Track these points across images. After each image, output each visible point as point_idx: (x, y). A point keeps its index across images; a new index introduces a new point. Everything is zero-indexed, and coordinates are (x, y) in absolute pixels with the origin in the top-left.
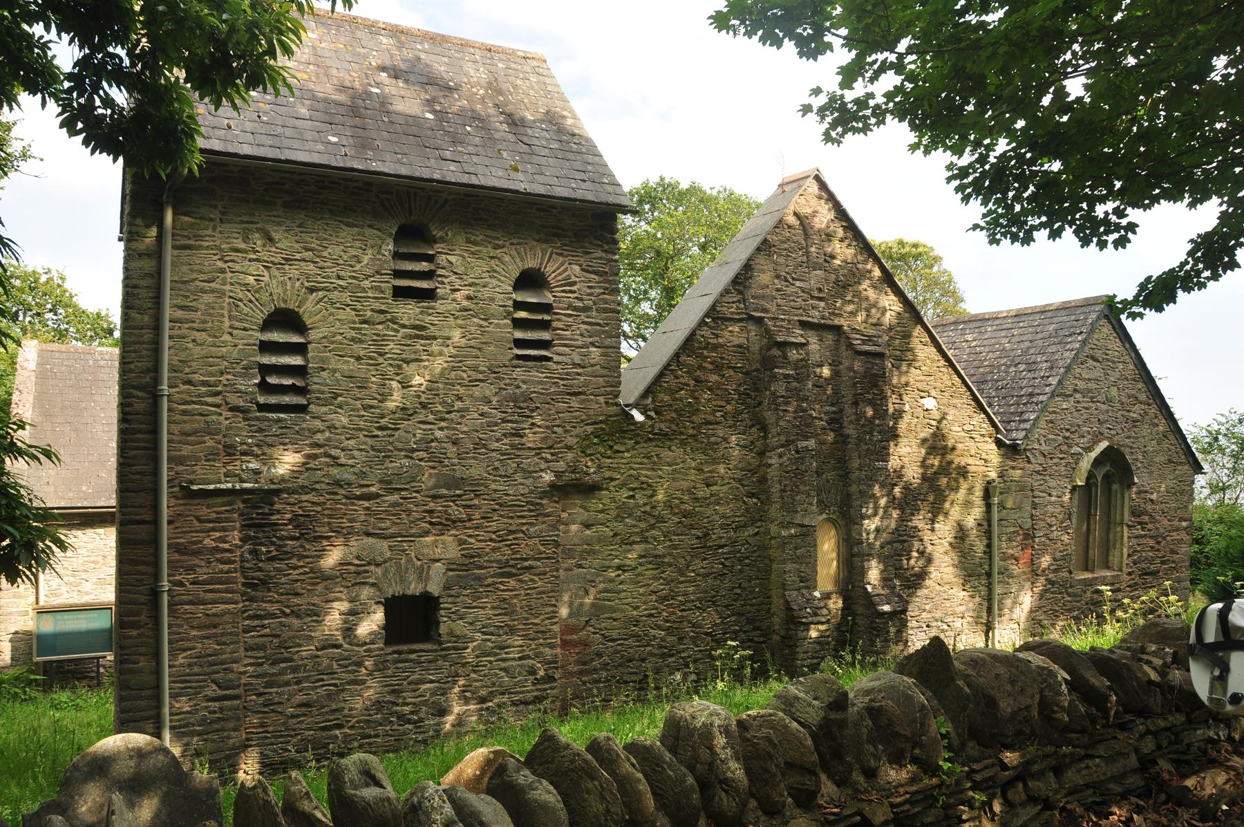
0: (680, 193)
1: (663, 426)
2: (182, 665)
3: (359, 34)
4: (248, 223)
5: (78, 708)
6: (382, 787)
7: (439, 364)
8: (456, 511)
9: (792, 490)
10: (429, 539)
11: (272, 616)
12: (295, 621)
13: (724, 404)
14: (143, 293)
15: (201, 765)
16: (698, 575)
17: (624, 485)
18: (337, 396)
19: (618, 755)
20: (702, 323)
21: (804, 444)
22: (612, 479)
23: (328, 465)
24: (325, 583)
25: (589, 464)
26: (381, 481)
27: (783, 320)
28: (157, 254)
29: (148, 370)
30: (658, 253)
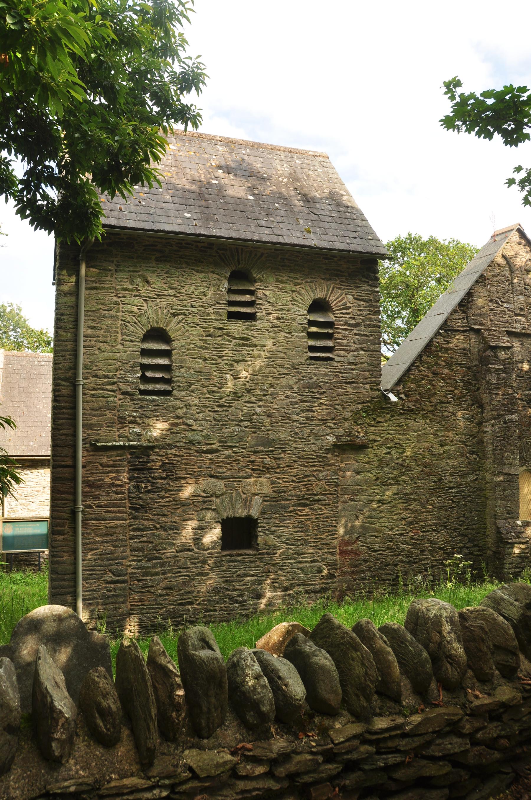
0: (422, 244)
1: (410, 404)
2: (90, 560)
3: (204, 145)
4: (133, 271)
5: (27, 584)
6: (213, 650)
7: (258, 363)
8: (268, 461)
9: (501, 450)
10: (252, 480)
11: (148, 529)
12: (163, 533)
13: (453, 389)
14: (67, 318)
15: (101, 625)
16: (434, 507)
17: (383, 445)
18: (191, 384)
19: (374, 635)
20: (437, 334)
21: (510, 417)
22: (375, 441)
23: (185, 430)
24: (182, 508)
25: (360, 430)
26: (220, 441)
27: (495, 331)
28: (76, 293)
29: (70, 368)
30: (407, 286)
